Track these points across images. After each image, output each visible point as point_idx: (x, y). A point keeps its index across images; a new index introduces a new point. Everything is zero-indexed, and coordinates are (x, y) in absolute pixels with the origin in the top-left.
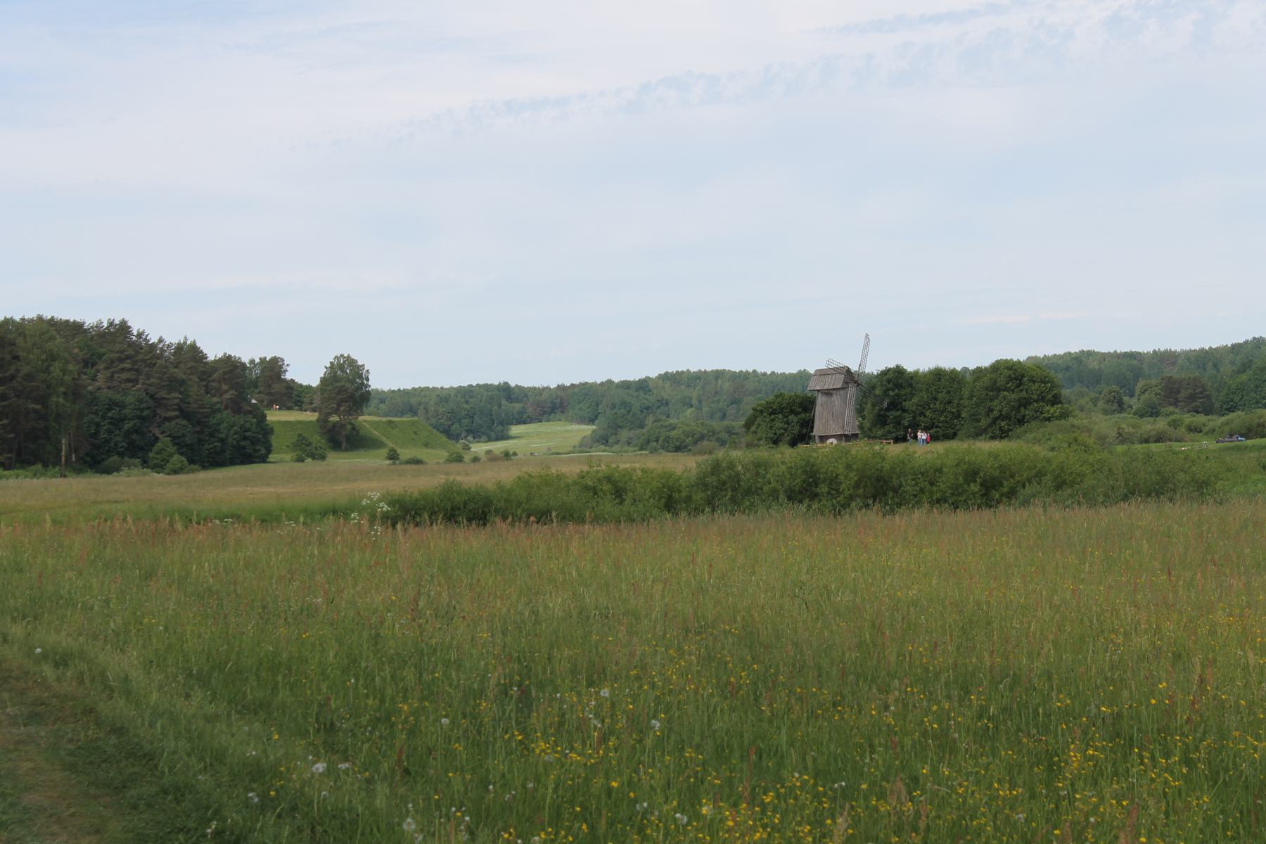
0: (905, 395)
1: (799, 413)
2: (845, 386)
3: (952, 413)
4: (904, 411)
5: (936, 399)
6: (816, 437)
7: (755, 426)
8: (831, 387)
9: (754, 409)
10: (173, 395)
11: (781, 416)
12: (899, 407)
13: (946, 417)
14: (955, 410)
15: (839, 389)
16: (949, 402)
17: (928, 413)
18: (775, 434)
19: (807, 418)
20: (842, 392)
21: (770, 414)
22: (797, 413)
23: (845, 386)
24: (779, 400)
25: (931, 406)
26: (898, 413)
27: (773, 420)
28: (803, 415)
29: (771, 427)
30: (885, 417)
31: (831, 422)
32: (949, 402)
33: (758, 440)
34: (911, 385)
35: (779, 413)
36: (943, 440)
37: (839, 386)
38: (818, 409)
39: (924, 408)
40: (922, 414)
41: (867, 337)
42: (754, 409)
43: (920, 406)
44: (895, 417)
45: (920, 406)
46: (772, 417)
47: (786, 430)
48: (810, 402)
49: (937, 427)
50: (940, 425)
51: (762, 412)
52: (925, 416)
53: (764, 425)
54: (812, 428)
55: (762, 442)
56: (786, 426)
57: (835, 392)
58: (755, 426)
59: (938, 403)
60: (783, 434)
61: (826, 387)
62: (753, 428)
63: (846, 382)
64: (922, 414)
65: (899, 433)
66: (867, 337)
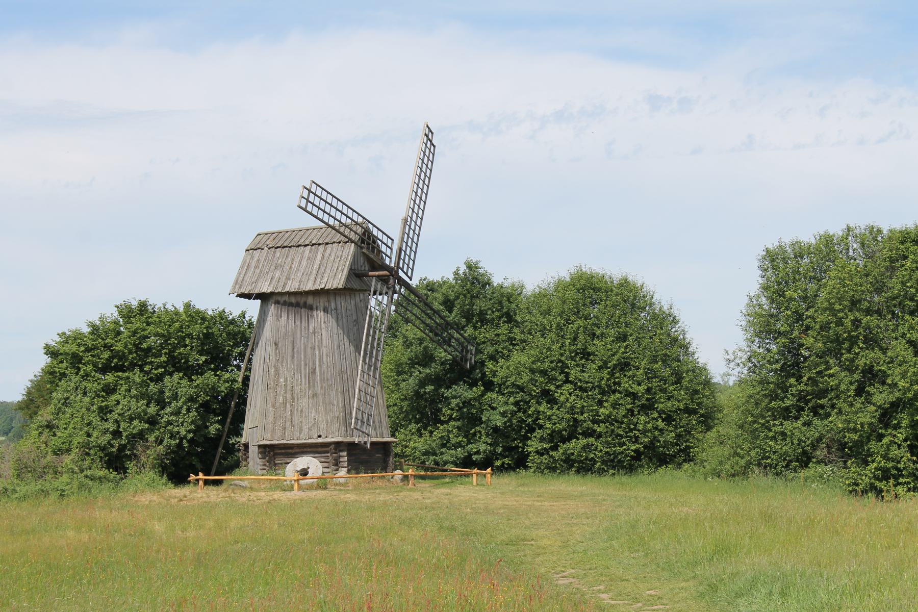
0: (494, 343)
1: (199, 370)
2: (356, 285)
3: (634, 396)
4: (489, 386)
5: (586, 355)
6: (253, 451)
7: (51, 408)
8: (309, 287)
9: (52, 352)
10: (396, 472)
11: (136, 376)
12: (477, 374)
13: (615, 405)
14: (642, 389)
15: (336, 292)
16: (624, 366)
17: (564, 394)
18: (117, 434)
19: (223, 388)
20: (345, 304)
21: (105, 370)
22: (190, 371)
23: (356, 285)
24: (137, 324)
25: (573, 373)
26: (478, 390)
27: (109, 390)
28: (210, 378)
29: (104, 412)
30: (436, 400)
31: (304, 402)
32: (624, 366)
33: (58, 452)
34: (510, 318)
35: (133, 366)
36: (601, 472)
37: (338, 281)
38: (262, 356)
39: (552, 380)
40: (547, 396)
41: (429, 135)
42: (52, 352)
43: (544, 373)
44: (467, 403)
45: (544, 373)
46: (110, 378)
47: (153, 422)
48: (232, 335)
49: (588, 433)
50: (600, 429)
51: (76, 360)
52: (552, 401)
53: (81, 402)
54: (240, 417)
55: (67, 459)
56: (152, 409)
57: (322, 302)
58: (51, 408)
59: (592, 367)
60: (141, 435)
61: (291, 287)
62: (45, 415)
63: (355, 274)
64: (547, 396)
65: (472, 447)
66: (429, 135)
